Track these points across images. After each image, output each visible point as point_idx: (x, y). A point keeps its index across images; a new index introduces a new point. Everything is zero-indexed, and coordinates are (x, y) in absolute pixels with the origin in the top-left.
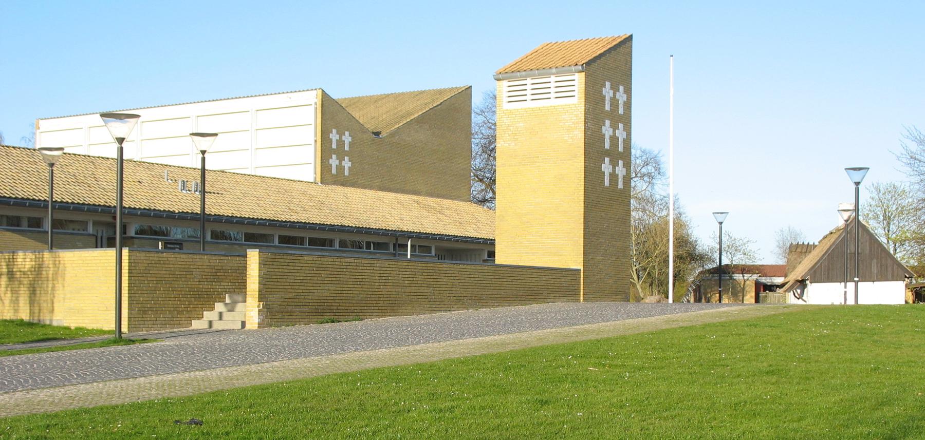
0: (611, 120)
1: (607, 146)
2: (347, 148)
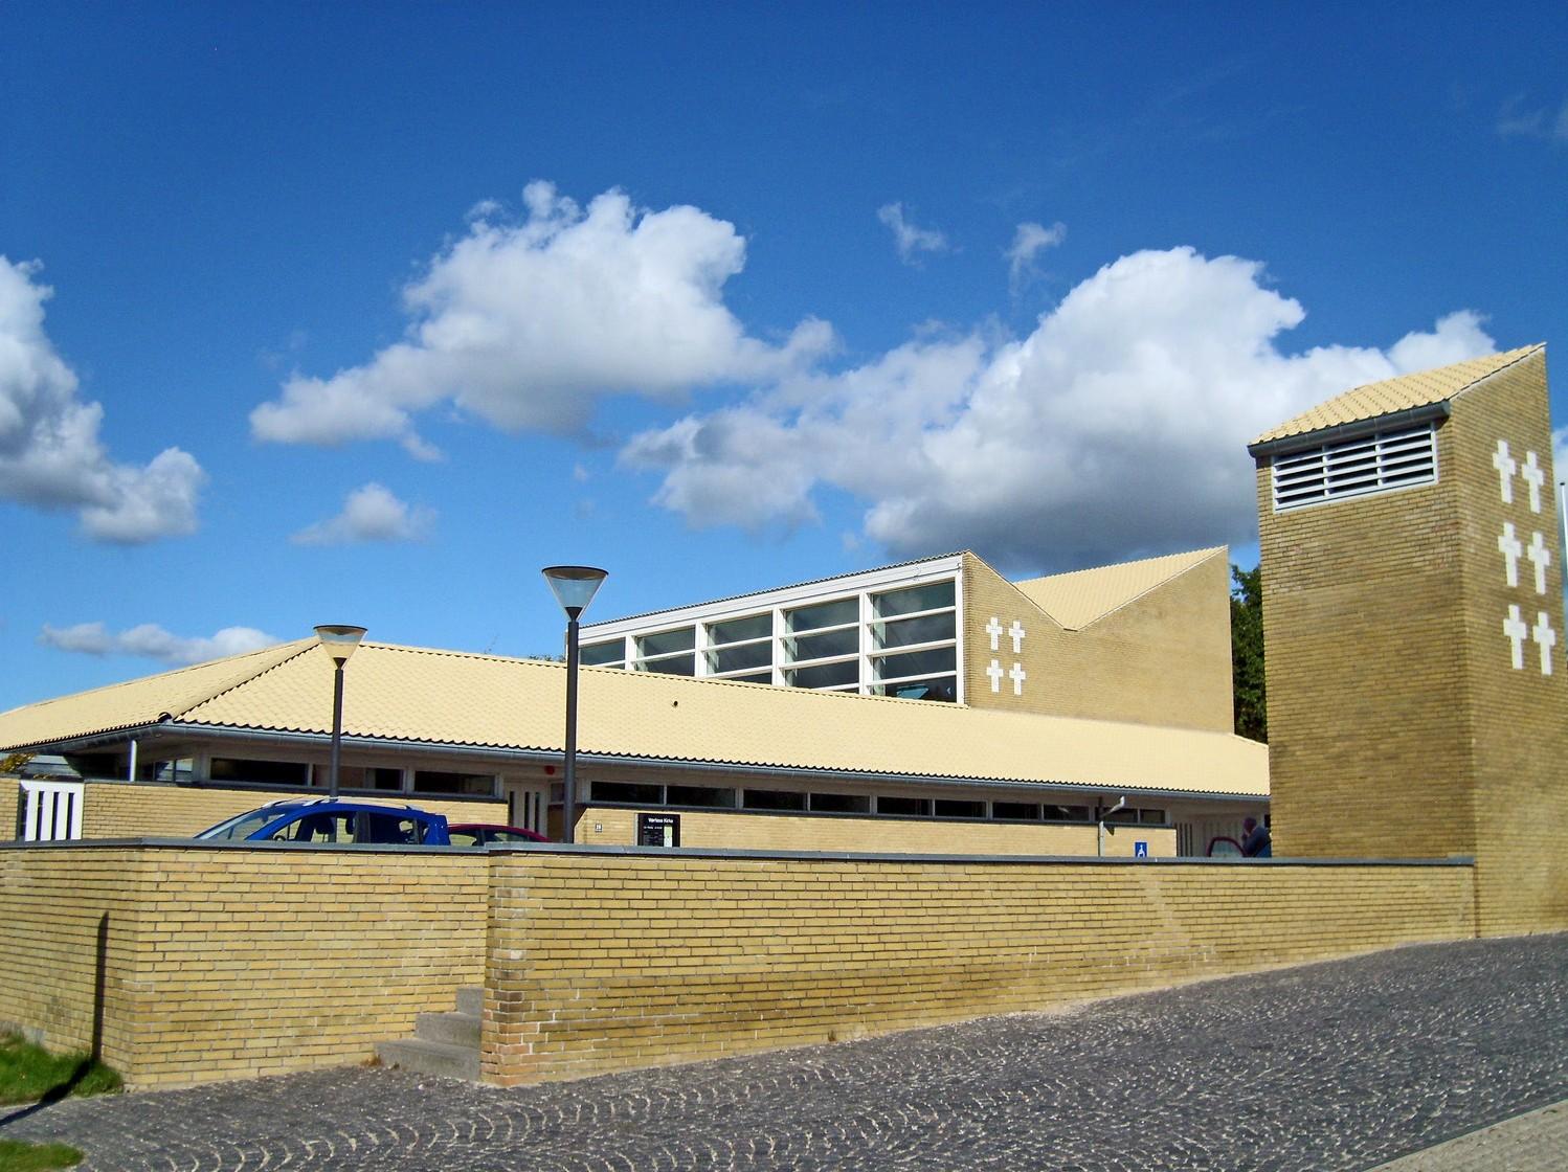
0: (1517, 523)
1: (1512, 580)
2: (1017, 649)
